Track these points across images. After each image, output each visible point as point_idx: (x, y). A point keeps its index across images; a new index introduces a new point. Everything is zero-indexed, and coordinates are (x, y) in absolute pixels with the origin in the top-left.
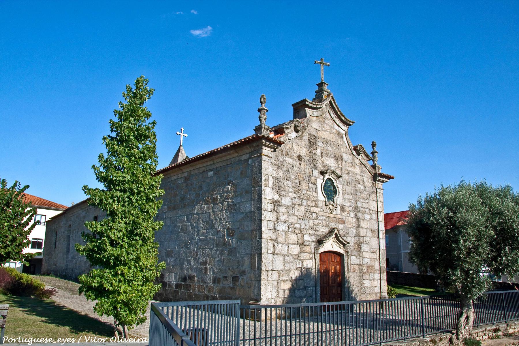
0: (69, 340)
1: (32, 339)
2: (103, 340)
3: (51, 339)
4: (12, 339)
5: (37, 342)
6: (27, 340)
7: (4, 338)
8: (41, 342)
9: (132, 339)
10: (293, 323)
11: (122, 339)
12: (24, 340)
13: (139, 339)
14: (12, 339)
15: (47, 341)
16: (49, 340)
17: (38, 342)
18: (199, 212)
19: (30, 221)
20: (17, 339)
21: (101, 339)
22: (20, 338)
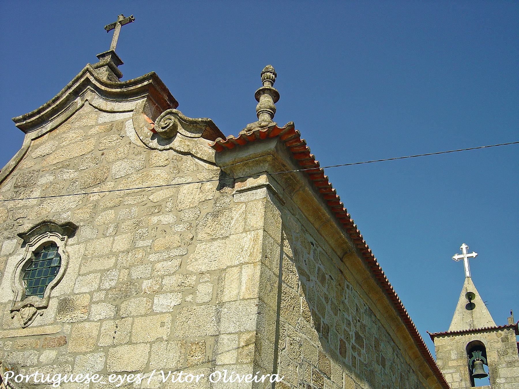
0: (80, 378)
1: (60, 375)
2: (195, 379)
3: (113, 376)
4: (22, 377)
5: (70, 381)
6: (50, 379)
7: (8, 375)
8: (77, 381)
9: (115, 375)
10: (477, 353)
11: (231, 377)
12: (45, 378)
13: (263, 376)
14: (193, 377)
15: (89, 380)
16: (93, 378)
17: (72, 381)
18: (192, 178)
19: (213, 147)
20: (32, 375)
21: (193, 377)
22: (37, 373)
